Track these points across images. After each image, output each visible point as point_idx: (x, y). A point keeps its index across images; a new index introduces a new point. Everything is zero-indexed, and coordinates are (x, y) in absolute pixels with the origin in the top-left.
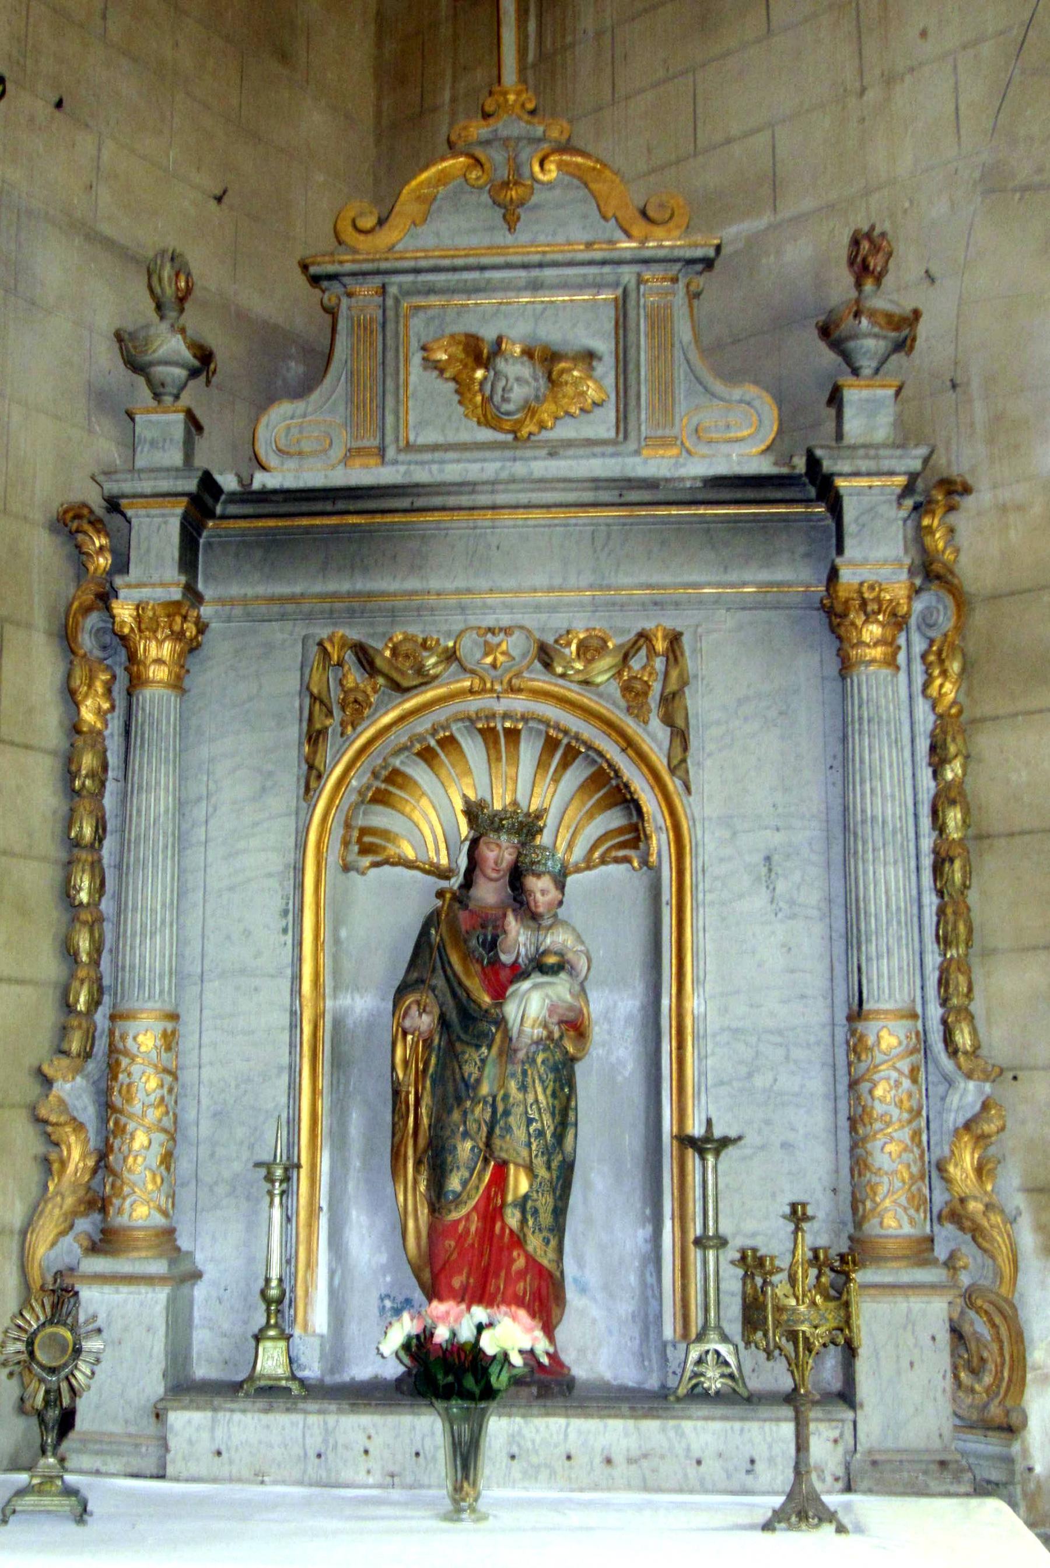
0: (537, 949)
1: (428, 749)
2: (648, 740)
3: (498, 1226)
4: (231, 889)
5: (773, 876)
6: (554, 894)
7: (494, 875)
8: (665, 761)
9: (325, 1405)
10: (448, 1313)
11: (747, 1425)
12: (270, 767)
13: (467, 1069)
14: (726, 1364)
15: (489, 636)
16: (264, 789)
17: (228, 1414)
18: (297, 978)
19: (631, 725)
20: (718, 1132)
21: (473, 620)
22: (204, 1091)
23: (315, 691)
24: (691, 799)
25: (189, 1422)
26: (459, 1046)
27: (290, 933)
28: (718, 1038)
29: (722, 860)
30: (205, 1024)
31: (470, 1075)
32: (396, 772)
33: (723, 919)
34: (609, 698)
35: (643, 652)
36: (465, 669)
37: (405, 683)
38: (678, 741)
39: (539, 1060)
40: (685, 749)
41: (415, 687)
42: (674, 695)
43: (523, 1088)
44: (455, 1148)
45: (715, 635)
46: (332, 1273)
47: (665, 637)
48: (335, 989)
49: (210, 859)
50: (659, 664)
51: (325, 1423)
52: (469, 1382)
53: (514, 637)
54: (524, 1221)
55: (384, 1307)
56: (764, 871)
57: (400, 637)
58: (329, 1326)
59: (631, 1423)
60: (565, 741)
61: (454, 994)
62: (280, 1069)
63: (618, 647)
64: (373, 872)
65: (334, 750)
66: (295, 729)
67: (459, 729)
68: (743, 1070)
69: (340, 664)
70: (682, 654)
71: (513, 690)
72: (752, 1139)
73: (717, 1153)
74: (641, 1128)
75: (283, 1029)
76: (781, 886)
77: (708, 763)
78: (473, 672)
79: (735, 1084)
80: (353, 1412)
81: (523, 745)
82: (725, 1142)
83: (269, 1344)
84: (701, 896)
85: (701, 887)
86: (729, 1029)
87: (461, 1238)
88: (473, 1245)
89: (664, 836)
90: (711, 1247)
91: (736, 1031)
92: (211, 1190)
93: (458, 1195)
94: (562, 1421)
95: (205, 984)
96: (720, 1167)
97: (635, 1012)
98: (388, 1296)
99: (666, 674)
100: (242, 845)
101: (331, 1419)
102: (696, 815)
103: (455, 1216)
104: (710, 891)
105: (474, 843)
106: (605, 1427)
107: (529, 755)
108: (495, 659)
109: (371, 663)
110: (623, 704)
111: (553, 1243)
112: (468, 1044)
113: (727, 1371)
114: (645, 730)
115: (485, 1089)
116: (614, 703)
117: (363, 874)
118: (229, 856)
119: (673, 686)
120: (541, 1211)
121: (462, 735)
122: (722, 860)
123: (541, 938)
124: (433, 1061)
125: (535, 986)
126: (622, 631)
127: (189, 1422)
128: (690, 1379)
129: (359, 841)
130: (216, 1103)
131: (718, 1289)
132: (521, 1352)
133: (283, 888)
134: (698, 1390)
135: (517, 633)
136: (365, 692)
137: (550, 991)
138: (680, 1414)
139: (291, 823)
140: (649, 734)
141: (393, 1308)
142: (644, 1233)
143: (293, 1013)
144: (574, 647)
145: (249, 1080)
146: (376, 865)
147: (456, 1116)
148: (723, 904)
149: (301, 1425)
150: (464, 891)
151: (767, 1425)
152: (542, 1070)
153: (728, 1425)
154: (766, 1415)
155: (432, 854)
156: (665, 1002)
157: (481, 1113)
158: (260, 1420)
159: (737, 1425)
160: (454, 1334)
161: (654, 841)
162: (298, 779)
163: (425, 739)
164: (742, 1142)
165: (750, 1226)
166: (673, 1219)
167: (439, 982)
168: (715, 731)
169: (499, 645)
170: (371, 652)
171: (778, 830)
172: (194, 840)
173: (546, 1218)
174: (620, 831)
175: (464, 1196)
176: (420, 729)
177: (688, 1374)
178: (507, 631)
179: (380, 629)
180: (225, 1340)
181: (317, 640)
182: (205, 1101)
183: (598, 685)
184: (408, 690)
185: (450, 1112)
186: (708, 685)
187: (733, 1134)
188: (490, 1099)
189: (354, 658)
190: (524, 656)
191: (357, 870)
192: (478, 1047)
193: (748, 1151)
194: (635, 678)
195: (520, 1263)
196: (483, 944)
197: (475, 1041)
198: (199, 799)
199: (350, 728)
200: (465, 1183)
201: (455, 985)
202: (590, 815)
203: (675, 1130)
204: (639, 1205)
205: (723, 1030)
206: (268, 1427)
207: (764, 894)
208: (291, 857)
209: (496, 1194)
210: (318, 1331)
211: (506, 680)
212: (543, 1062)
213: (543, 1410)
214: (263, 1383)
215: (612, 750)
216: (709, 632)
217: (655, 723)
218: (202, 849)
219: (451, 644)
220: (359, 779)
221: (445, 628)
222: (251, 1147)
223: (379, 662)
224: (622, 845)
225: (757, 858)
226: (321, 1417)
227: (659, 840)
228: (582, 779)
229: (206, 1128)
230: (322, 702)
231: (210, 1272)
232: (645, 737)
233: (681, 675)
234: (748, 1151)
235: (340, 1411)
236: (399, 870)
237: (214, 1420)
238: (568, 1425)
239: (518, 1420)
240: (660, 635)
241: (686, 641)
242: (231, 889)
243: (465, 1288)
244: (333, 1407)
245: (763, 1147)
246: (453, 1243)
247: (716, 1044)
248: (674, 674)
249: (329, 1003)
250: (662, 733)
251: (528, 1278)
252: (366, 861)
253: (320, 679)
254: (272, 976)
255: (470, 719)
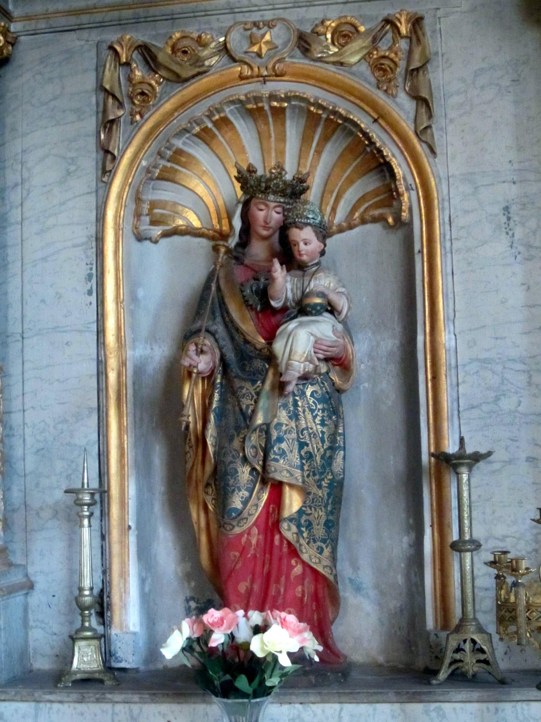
0: (303, 293)
1: (206, 130)
2: (397, 109)
3: (277, 537)
4: (44, 259)
5: (512, 223)
6: (315, 245)
7: (265, 233)
8: (412, 127)
9: (129, 696)
10: (222, 620)
11: (501, 705)
12: (73, 154)
13: (246, 402)
14: (482, 651)
15: (254, 30)
16: (69, 173)
17: (48, 705)
18: (101, 332)
19: (380, 97)
20: (469, 450)
21: (240, 17)
22: (28, 431)
23: (107, 87)
24: (436, 160)
25: (16, 710)
26: (237, 383)
27: (94, 294)
28: (467, 368)
29: (466, 212)
30: (26, 376)
31: (248, 406)
32: (179, 152)
33: (469, 264)
34: (361, 75)
35: (390, 35)
36: (234, 60)
37: (185, 74)
38: (423, 110)
39: (308, 393)
40: (430, 116)
41: (193, 77)
42: (417, 69)
43: (295, 416)
44: (237, 472)
45: (451, 18)
46: (142, 581)
47: (408, 21)
48: (134, 341)
49: (25, 236)
50: (403, 45)
51: (131, 711)
52: (242, 682)
53: (276, 29)
54: (300, 533)
55: (190, 607)
56: (504, 219)
57: (178, 35)
58: (141, 625)
59: (397, 706)
60: (324, 116)
61: (232, 339)
62: (90, 409)
63: (368, 32)
64: (164, 242)
65: (126, 135)
66: (94, 119)
67: (231, 111)
68: (492, 395)
69: (128, 64)
70: (424, 35)
71: (279, 75)
72: (499, 455)
73: (470, 467)
74: (402, 449)
75: (91, 376)
76: (519, 232)
77: (450, 128)
78: (243, 62)
79: (485, 408)
80: (153, 701)
81: (288, 123)
82: (477, 458)
83: (82, 643)
84: (448, 244)
85: (448, 237)
86: (478, 360)
87: (243, 551)
88: (255, 556)
89: (413, 193)
90: (468, 550)
91: (485, 361)
92: (38, 514)
93: (240, 513)
94: (337, 706)
95: (26, 342)
96: (472, 480)
97: (395, 349)
98: (192, 598)
99: (410, 52)
100: (51, 221)
101: (135, 708)
102: (442, 174)
103: (237, 530)
104: (457, 239)
105: (246, 205)
106: (375, 709)
107: (294, 132)
108: (260, 48)
109: (154, 58)
110: (373, 80)
111: (327, 552)
112: (245, 380)
113: (482, 657)
114: (394, 101)
115: (259, 420)
116: (366, 80)
117: (156, 242)
118: (41, 233)
119: (416, 64)
120: (315, 523)
121: (236, 118)
122: (466, 212)
123: (306, 283)
124: (216, 397)
125: (301, 324)
126: (370, 19)
127: (16, 710)
128: (451, 664)
129: (150, 213)
130: (38, 441)
131: (473, 586)
132: (290, 654)
133: (87, 257)
134: (459, 671)
135: (279, 26)
136: (150, 85)
137: (314, 329)
138: (441, 698)
139: (92, 199)
140: (397, 104)
141: (197, 608)
142: (406, 540)
143: (99, 362)
144: (329, 36)
145: (65, 421)
146: (166, 235)
147: (236, 443)
148: (469, 250)
149: (110, 712)
150: (240, 250)
151: (519, 705)
152: (311, 402)
153: (484, 706)
154: (518, 697)
155: (215, 222)
156: (420, 338)
157: (254, 439)
158: (75, 708)
159: (492, 706)
160: (232, 637)
161: (405, 198)
162: (97, 163)
163: (203, 122)
164: (491, 458)
165: (500, 530)
166: (432, 526)
167: (220, 328)
168: (455, 100)
169: (263, 36)
170: (153, 49)
171: (514, 183)
172: (12, 220)
173: (319, 531)
174: (375, 193)
175: (245, 514)
176: (198, 114)
177: (447, 661)
178: (270, 25)
179: (162, 31)
180: (55, 637)
181: (109, 44)
182: (29, 440)
183: (351, 65)
184: (186, 80)
185: (231, 440)
186: (447, 60)
187: (483, 450)
188: (265, 427)
189: (140, 57)
190: (285, 45)
191: (150, 239)
192: (254, 382)
193: (496, 466)
194: (384, 57)
195: (298, 570)
196: (257, 293)
197: (251, 377)
198: (16, 185)
199: (138, 117)
200: (245, 503)
201: (233, 331)
202: (350, 181)
203: (432, 450)
204: (403, 516)
205: (472, 360)
206: (82, 714)
207: (505, 240)
208: (93, 230)
209: (274, 509)
210: (132, 629)
211: (270, 66)
212: (312, 395)
213: (318, 699)
214: (79, 676)
215: (364, 122)
216: (446, 16)
217: (403, 98)
218: (20, 226)
219: (222, 39)
220: (147, 159)
221: (215, 25)
222: (68, 477)
223: (161, 57)
224: (377, 206)
225: (497, 209)
226: (127, 706)
227: (409, 198)
228: (340, 150)
229: (30, 464)
230: (114, 97)
231: (41, 583)
232: (393, 106)
233: (423, 52)
234: (496, 466)
235: (143, 701)
236: (188, 238)
237: (36, 710)
238: (341, 709)
239: (298, 706)
240: (403, 20)
241: (427, 22)
242: (44, 259)
243: (250, 592)
244: (136, 698)
245: (510, 462)
246: (237, 554)
247: (467, 373)
248: (417, 55)
249: (129, 353)
250: (409, 105)
251: (306, 582)
252: (157, 231)
253: (112, 76)
254: (81, 331)
255: (240, 101)
